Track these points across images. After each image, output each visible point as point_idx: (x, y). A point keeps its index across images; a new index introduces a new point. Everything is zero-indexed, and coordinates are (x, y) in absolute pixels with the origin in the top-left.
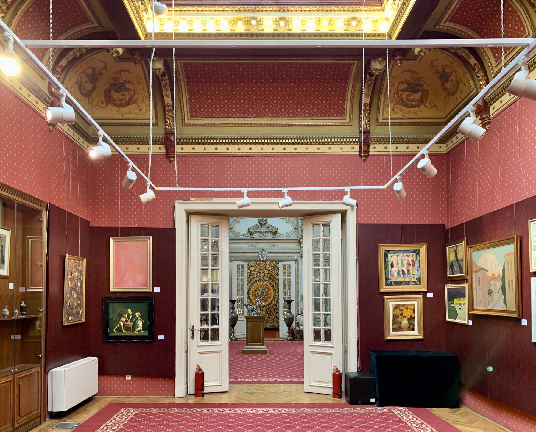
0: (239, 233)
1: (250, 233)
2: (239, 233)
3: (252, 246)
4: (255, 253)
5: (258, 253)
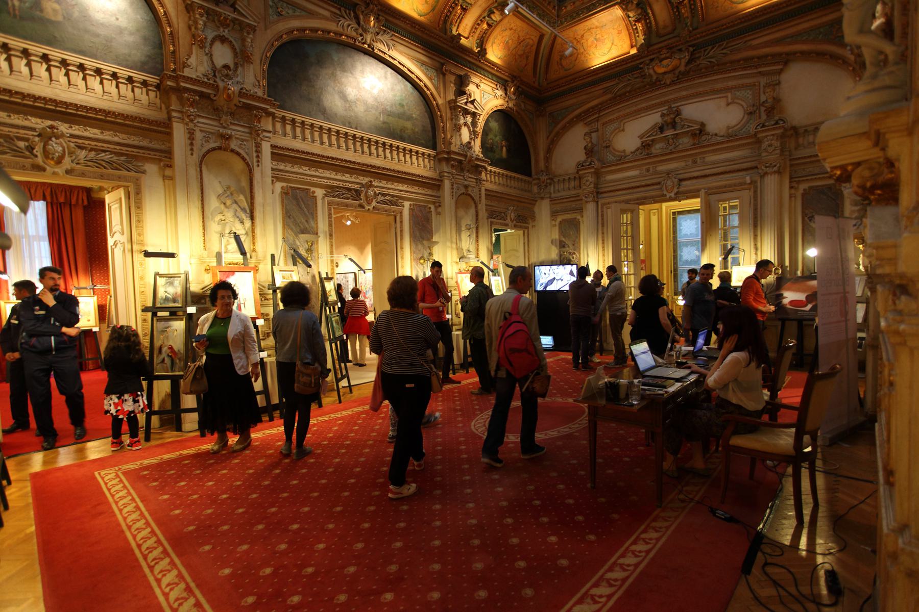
0: (624, 151)
1: (646, 146)
2: (624, 151)
3: (648, 170)
4: (639, 187)
5: (659, 183)
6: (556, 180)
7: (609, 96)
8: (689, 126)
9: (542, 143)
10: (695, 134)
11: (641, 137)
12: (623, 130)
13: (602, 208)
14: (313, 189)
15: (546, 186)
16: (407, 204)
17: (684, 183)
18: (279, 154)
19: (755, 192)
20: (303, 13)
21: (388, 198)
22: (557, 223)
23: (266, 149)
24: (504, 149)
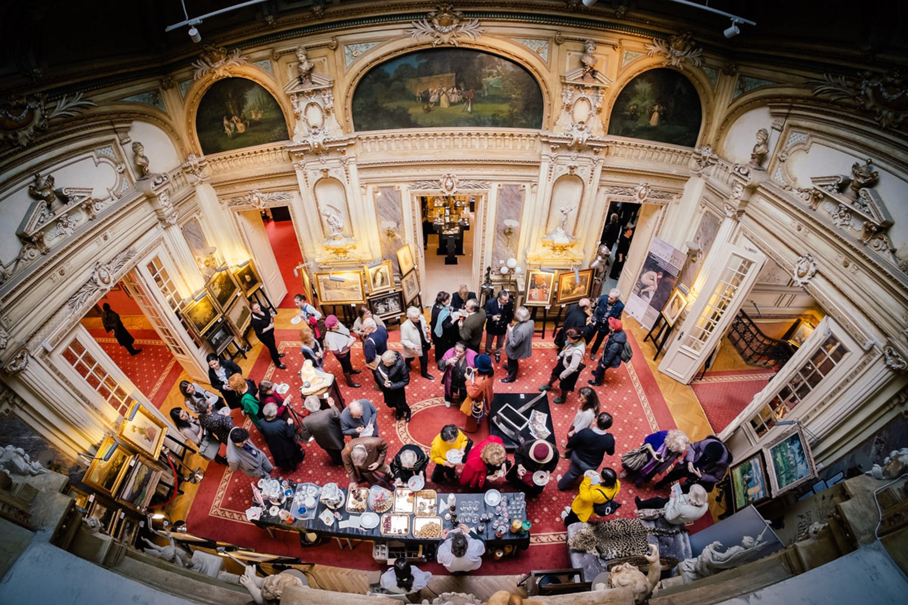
0: (795, 180)
6: (721, 162)
7: (807, 93)
8: (869, 213)
9: (720, 110)
10: (871, 231)
11: (815, 180)
12: (806, 151)
13: (739, 231)
14: (397, 185)
15: (707, 165)
16: (495, 186)
17: (819, 279)
18: (362, 168)
19: (864, 364)
20: (376, 44)
21: (471, 182)
22: (704, 211)
23: (353, 169)
24: (656, 115)
